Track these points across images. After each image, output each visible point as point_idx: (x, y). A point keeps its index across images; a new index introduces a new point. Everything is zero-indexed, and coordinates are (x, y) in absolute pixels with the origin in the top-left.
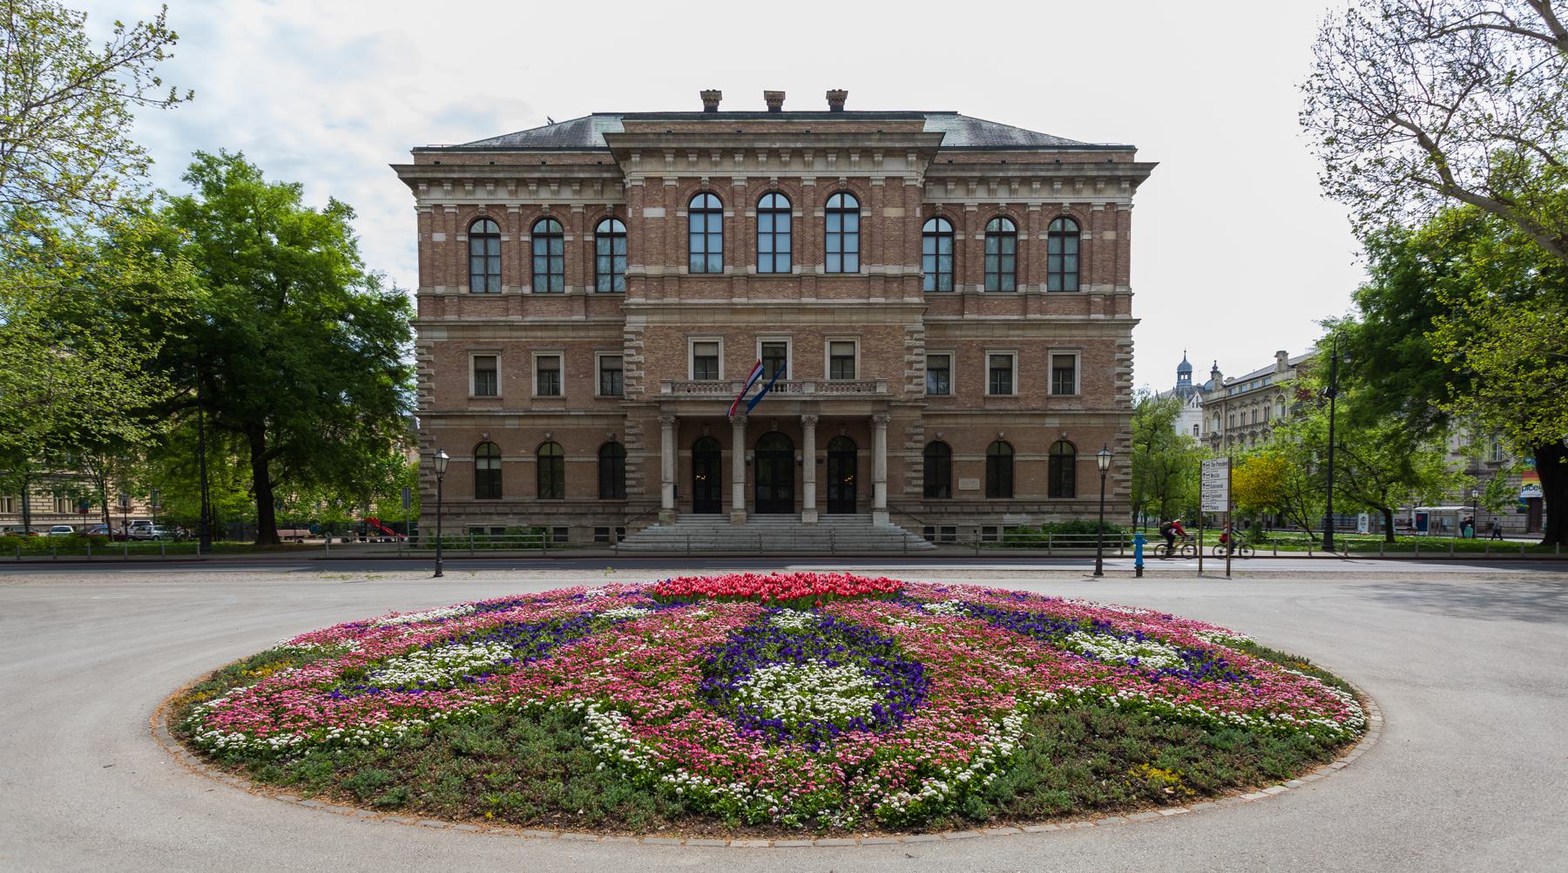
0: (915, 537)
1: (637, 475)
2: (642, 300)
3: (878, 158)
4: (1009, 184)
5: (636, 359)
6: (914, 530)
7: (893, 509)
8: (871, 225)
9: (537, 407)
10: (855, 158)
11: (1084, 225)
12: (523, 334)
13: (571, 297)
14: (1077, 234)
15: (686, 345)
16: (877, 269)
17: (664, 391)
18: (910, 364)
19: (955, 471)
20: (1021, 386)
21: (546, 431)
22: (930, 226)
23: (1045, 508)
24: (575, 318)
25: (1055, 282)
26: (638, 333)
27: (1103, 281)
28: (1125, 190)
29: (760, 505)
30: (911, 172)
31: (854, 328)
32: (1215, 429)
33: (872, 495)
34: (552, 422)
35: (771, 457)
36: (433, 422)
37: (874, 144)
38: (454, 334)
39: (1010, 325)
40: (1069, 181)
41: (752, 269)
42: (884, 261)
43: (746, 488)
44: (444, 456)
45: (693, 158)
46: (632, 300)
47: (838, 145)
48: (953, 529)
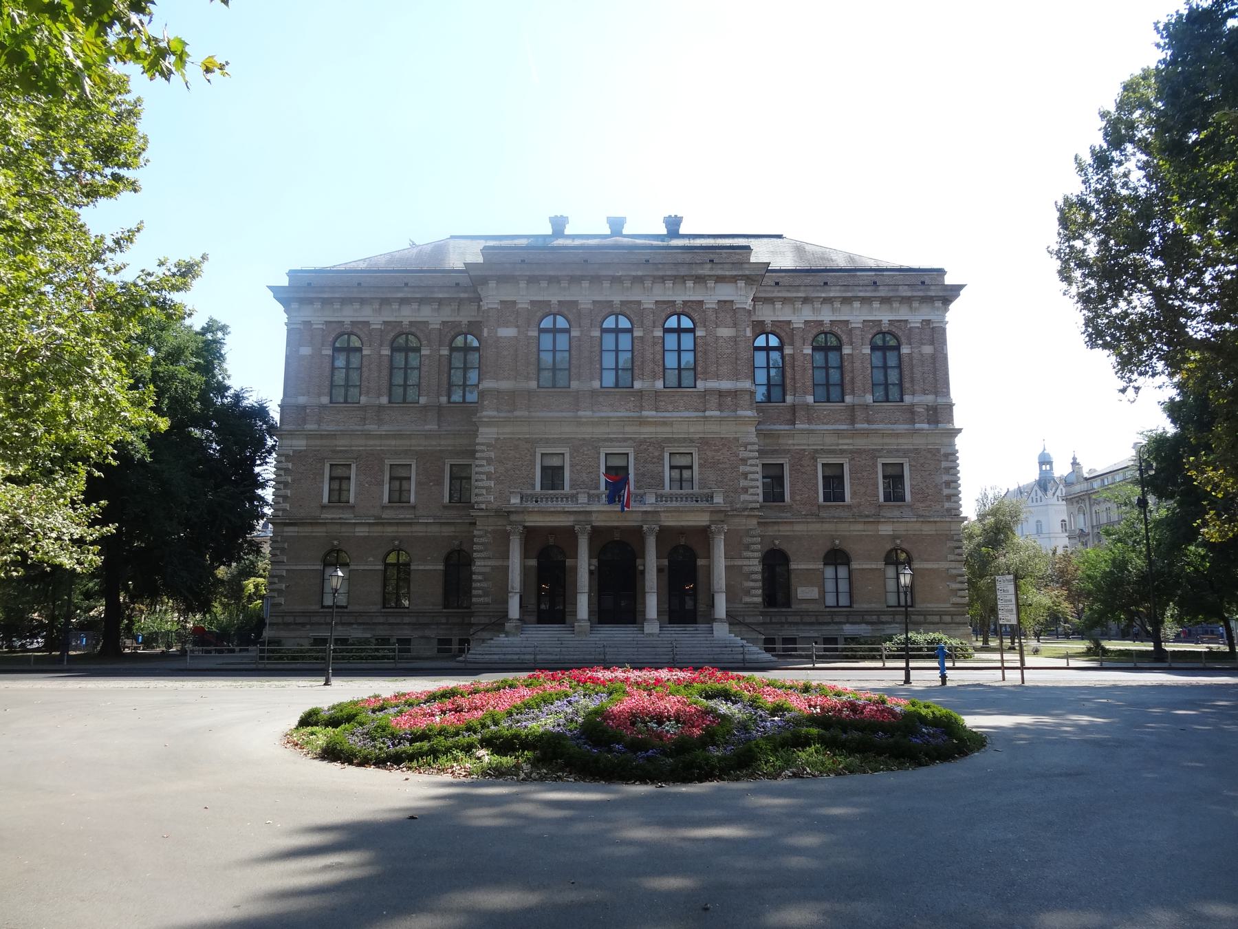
0: (755, 649)
1: (484, 585)
2: (495, 413)
3: (711, 284)
4: (832, 303)
5: (486, 469)
6: (754, 641)
7: (733, 619)
8: (705, 344)
9: (388, 515)
10: (690, 284)
11: (903, 340)
12: (377, 442)
13: (425, 407)
14: (898, 348)
15: (534, 455)
16: (712, 384)
17: (513, 501)
18: (745, 475)
19: (794, 580)
20: (854, 494)
21: (395, 538)
22: (761, 341)
23: (884, 618)
24: (427, 427)
25: (880, 393)
26: (489, 445)
27: (924, 392)
28: (938, 309)
29: (604, 615)
30: (742, 296)
31: (692, 441)
32: (1082, 526)
33: (711, 605)
34: (401, 529)
35: (621, 574)
36: (286, 529)
37: (707, 272)
38: (313, 442)
39: (838, 433)
40: (885, 300)
41: (596, 384)
42: (717, 377)
43: (590, 597)
44: (340, 574)
45: (544, 284)
46: (485, 413)
47: (674, 273)
48: (793, 641)
